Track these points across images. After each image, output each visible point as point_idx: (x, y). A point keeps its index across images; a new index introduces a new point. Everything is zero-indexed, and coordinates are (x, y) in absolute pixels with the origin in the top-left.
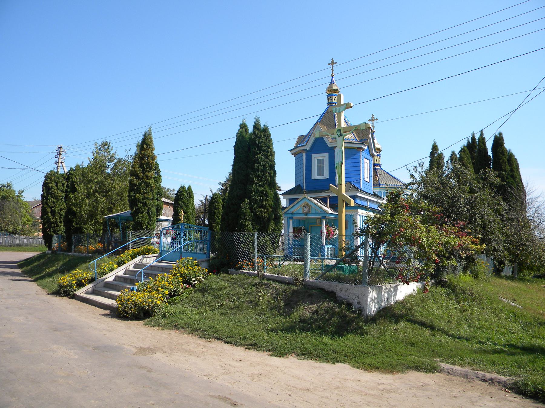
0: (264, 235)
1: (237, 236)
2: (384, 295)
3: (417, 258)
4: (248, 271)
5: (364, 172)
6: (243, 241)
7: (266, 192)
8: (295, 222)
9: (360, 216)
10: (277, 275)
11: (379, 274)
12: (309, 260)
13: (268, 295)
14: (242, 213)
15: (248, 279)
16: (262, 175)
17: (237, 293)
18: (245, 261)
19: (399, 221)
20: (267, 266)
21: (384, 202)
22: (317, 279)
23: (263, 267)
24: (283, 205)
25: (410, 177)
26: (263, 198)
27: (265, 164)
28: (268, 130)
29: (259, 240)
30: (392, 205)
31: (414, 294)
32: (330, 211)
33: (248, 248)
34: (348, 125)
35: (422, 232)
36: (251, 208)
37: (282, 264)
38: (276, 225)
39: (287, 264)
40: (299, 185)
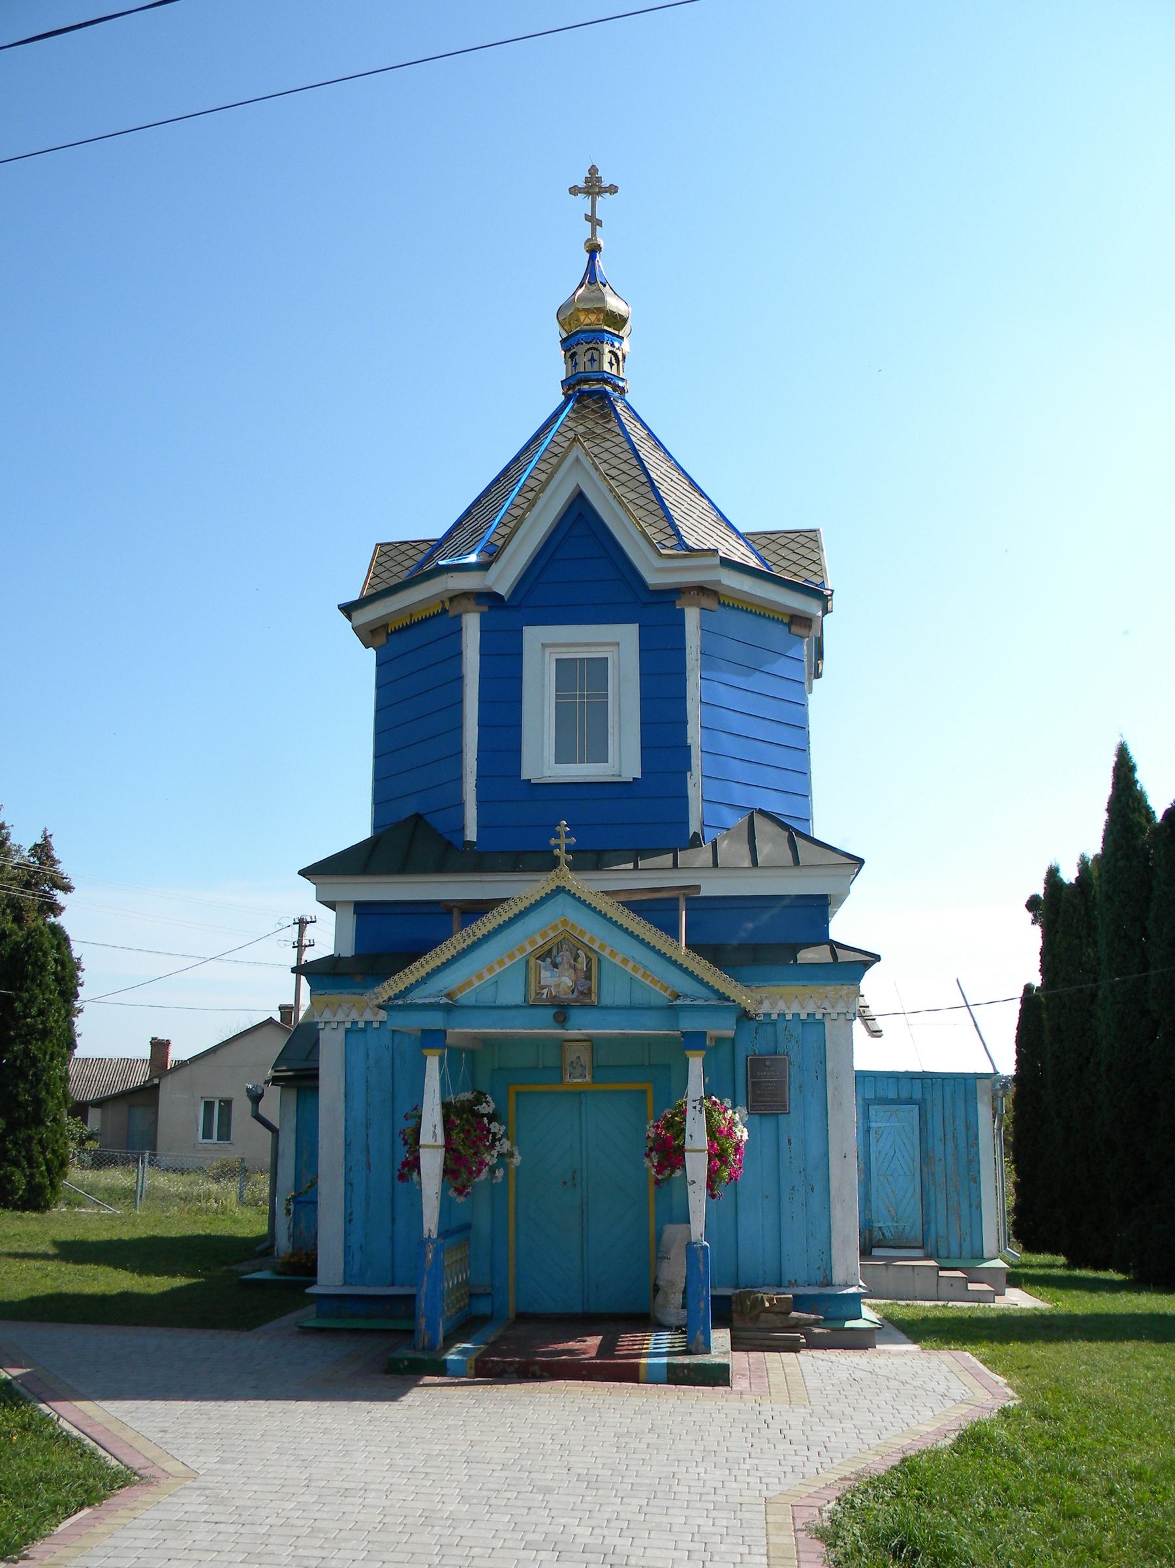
40: (418, 817)
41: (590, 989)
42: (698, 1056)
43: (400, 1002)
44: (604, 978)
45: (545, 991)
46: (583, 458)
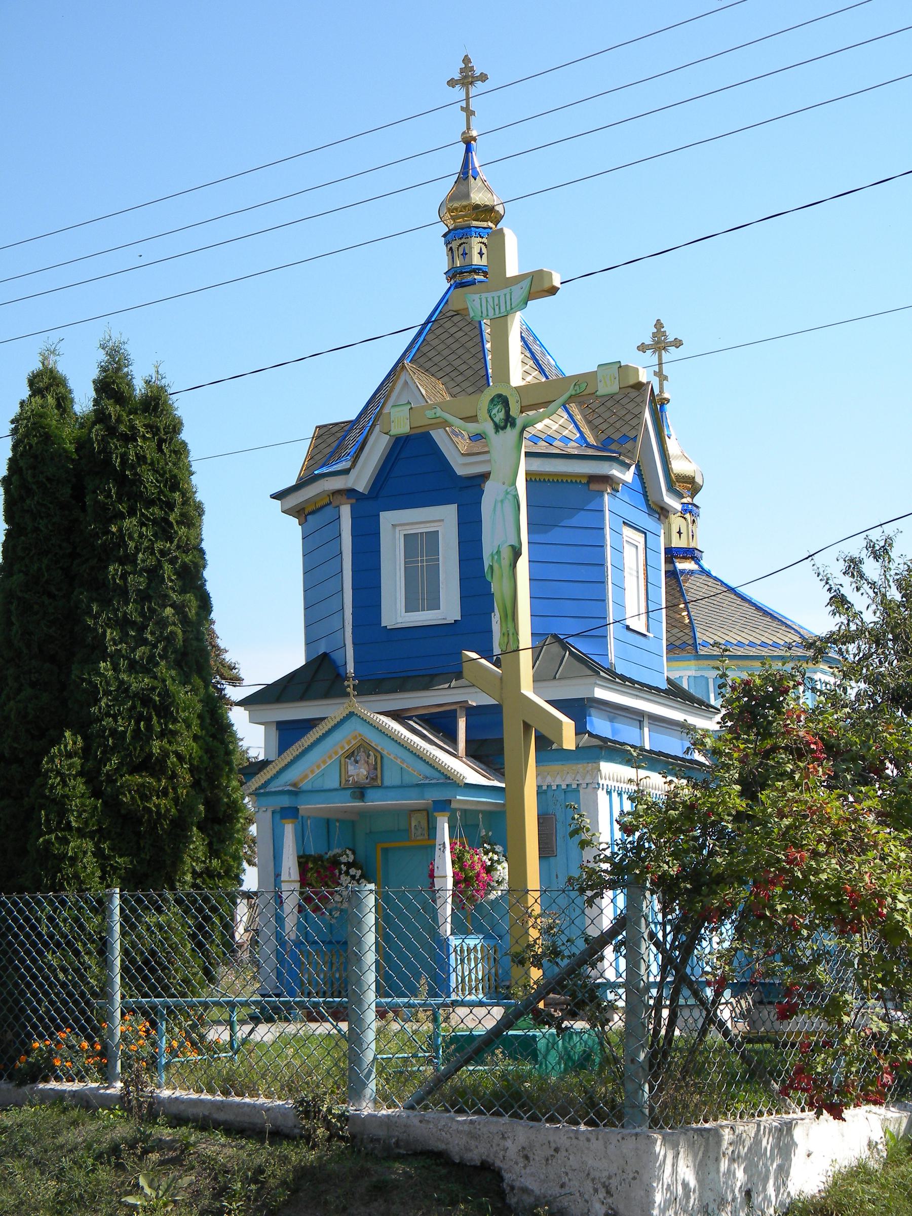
0: (154, 903)
1: (20, 911)
2: (730, 1173)
3: (875, 989)
4: (76, 1086)
5: (620, 588)
6: (51, 936)
7: (166, 694)
8: (308, 833)
9: (609, 793)
10: (219, 1098)
11: (700, 1071)
12: (371, 1015)
13: (175, 1202)
14: (47, 797)
15: (75, 1123)
16: (142, 614)
17: (22, 1203)
18: (60, 1036)
19: (782, 815)
20: (173, 1052)
21: (710, 724)
22: (411, 1108)
23: (153, 1063)
24: (252, 753)
25: (830, 608)
26: (149, 727)
27: (159, 561)
28: (165, 402)
29: (133, 927)
30: (747, 741)
31: (873, 1165)
32: (471, 775)
33: (77, 971)
34: (542, 371)
35: (891, 866)
36: (90, 776)
37: (245, 1041)
38: (213, 851)
39: (269, 1038)
40: (325, 655)
41: (377, 776)
42: (444, 816)
43: (262, 791)
44: (385, 768)
45: (351, 779)
46: (409, 382)
